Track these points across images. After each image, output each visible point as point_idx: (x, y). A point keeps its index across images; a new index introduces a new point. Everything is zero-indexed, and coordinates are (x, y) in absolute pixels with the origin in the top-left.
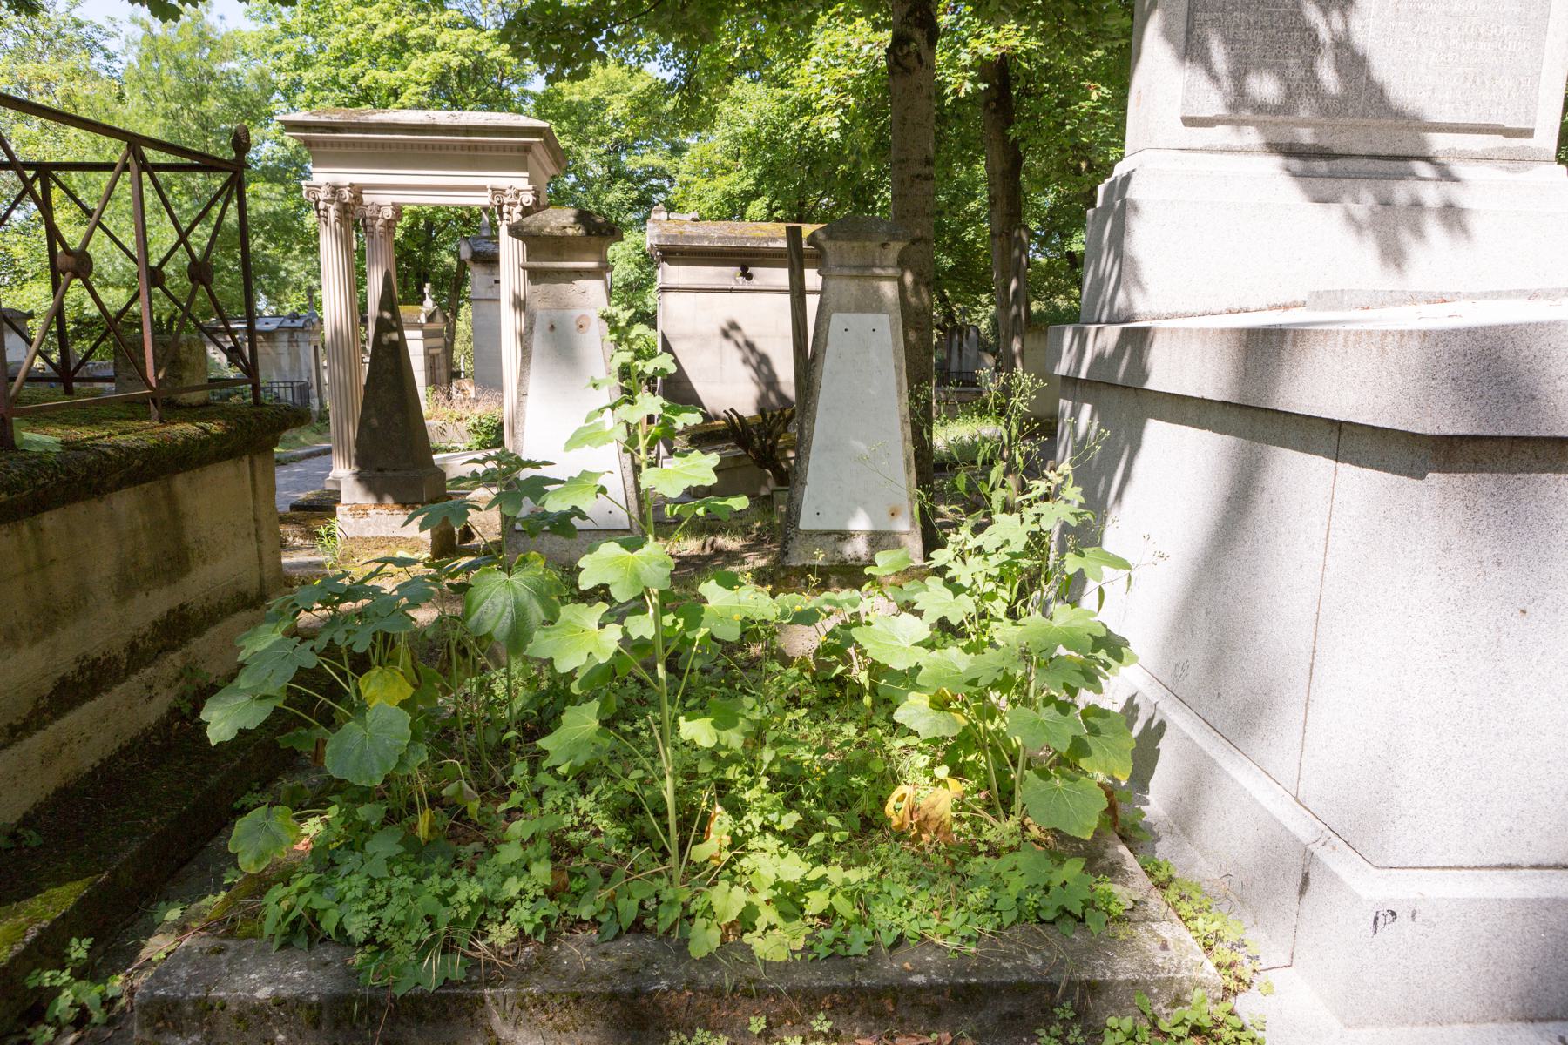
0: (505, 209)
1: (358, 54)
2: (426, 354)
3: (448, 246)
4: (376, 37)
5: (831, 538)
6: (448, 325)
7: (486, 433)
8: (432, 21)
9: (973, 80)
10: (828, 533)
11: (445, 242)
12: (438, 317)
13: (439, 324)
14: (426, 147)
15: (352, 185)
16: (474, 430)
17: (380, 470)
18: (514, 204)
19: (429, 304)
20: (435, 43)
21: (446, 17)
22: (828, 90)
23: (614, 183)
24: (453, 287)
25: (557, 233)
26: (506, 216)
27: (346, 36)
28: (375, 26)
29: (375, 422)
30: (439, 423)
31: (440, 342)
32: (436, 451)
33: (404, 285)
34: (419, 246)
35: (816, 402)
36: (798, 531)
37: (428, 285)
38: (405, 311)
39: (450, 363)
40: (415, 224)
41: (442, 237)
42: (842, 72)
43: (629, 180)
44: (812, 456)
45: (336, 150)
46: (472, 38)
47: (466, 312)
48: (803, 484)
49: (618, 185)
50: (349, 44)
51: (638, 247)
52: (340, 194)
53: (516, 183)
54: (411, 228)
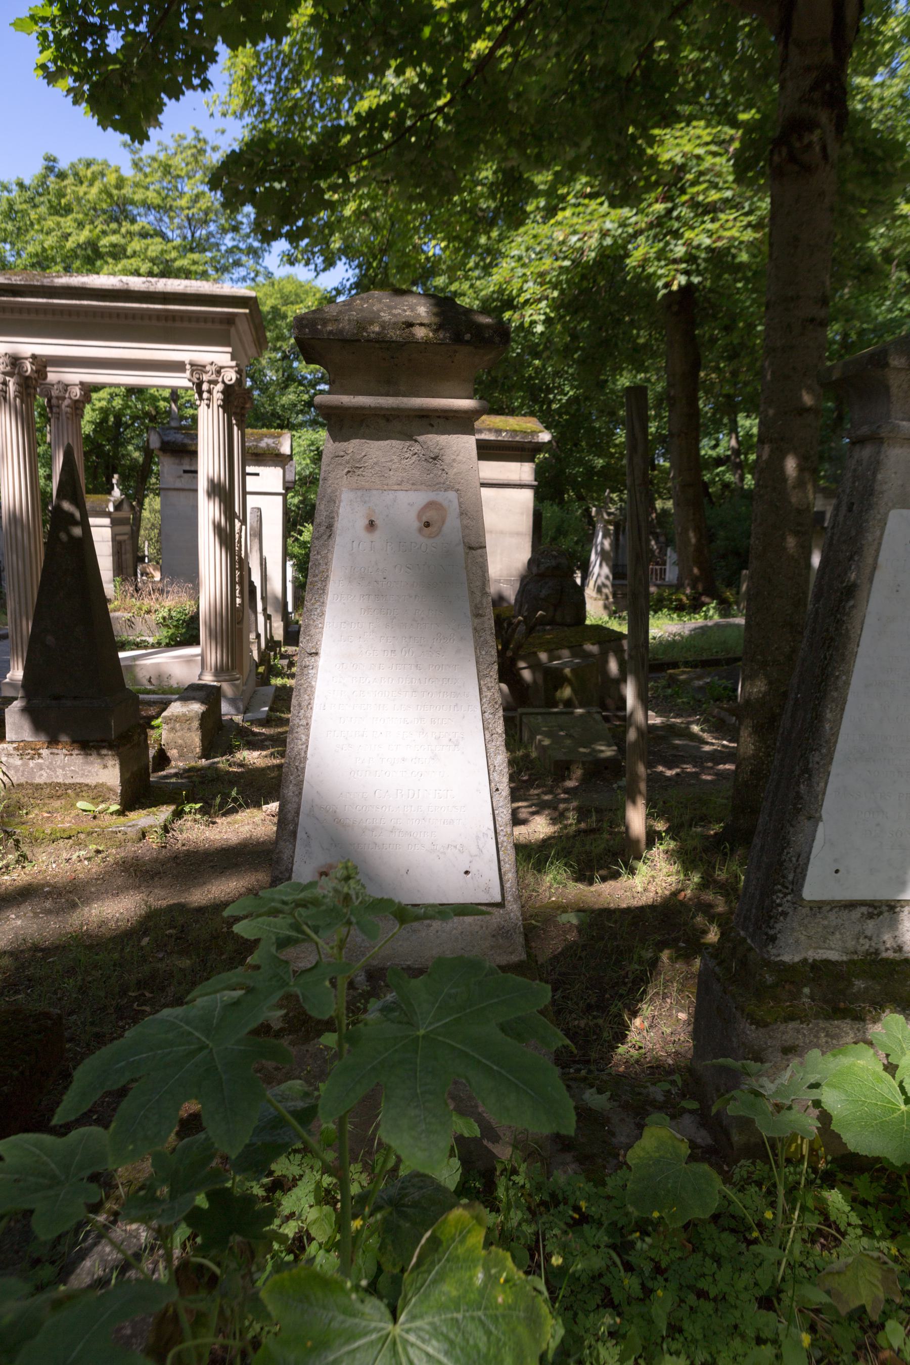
0: (205, 387)
1: (53, 260)
2: (114, 539)
3: (135, 441)
4: (70, 244)
5: (856, 914)
6: (135, 514)
7: (176, 627)
8: (123, 230)
9: (687, 273)
10: (851, 905)
11: (132, 438)
12: (126, 506)
13: (126, 513)
14: (118, 315)
15: (34, 357)
16: (164, 623)
17: (57, 698)
18: (215, 382)
19: (117, 493)
20: (125, 250)
21: (136, 228)
22: (530, 284)
23: (286, 387)
24: (138, 481)
25: (394, 334)
26: (205, 395)
27: (42, 243)
28: (69, 235)
29: (50, 639)
30: (128, 615)
31: (127, 529)
32: (124, 646)
33: (93, 473)
34: (108, 440)
35: (849, 673)
36: (799, 901)
37: (116, 476)
38: (91, 500)
39: (136, 548)
40: (104, 420)
41: (128, 434)
42: (547, 263)
43: (300, 384)
44: (834, 769)
45: (17, 316)
46: (160, 247)
47: (152, 504)
48: (815, 819)
49: (291, 389)
50: (44, 250)
51: (312, 444)
52: (21, 366)
53: (217, 357)
54: (101, 422)
